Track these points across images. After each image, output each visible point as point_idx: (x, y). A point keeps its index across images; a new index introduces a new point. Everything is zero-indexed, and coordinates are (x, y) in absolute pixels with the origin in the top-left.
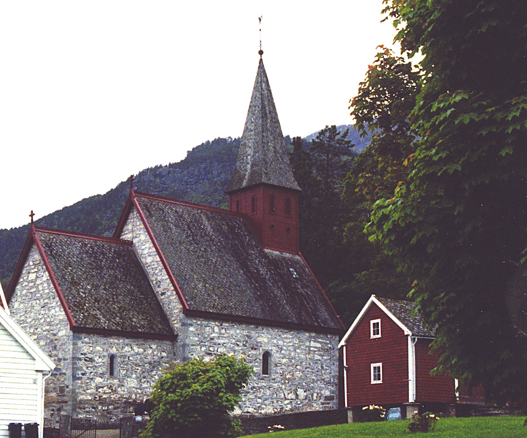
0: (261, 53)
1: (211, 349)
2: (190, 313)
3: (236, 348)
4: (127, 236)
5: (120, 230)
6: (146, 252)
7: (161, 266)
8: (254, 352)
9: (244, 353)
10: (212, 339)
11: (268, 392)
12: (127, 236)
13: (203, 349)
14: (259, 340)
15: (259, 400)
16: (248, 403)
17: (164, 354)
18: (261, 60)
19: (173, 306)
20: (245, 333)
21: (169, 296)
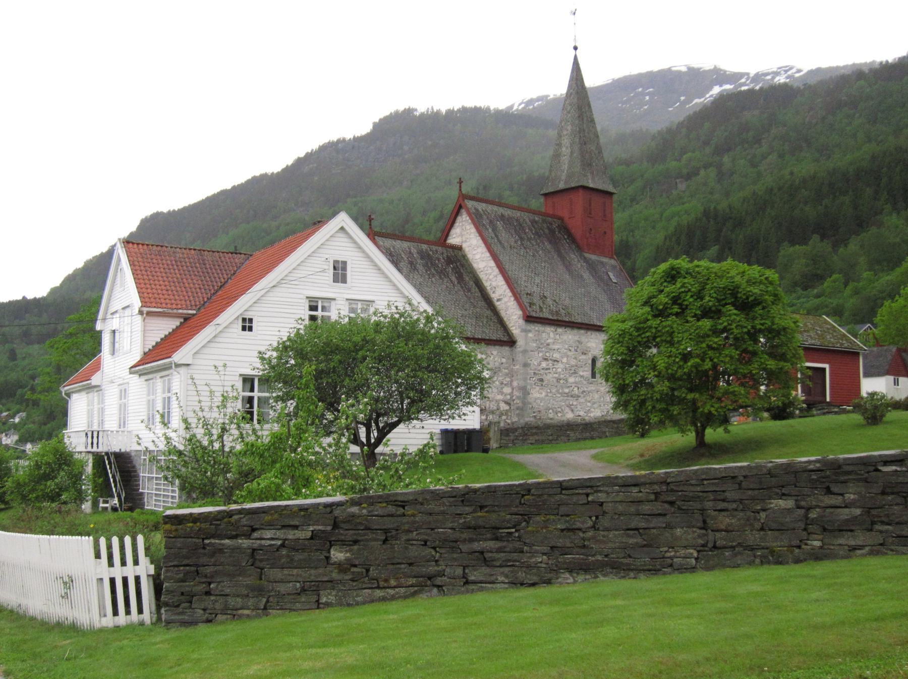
0: (576, 48)
1: (547, 354)
2: (529, 319)
3: (569, 353)
4: (454, 239)
5: (446, 233)
6: (478, 257)
7: (496, 271)
8: (584, 357)
9: (575, 358)
10: (548, 345)
11: (596, 396)
12: (454, 239)
13: (541, 354)
14: (589, 345)
15: (589, 404)
16: (579, 407)
17: (504, 360)
18: (576, 58)
19: (512, 313)
20: (576, 338)
21: (506, 303)
